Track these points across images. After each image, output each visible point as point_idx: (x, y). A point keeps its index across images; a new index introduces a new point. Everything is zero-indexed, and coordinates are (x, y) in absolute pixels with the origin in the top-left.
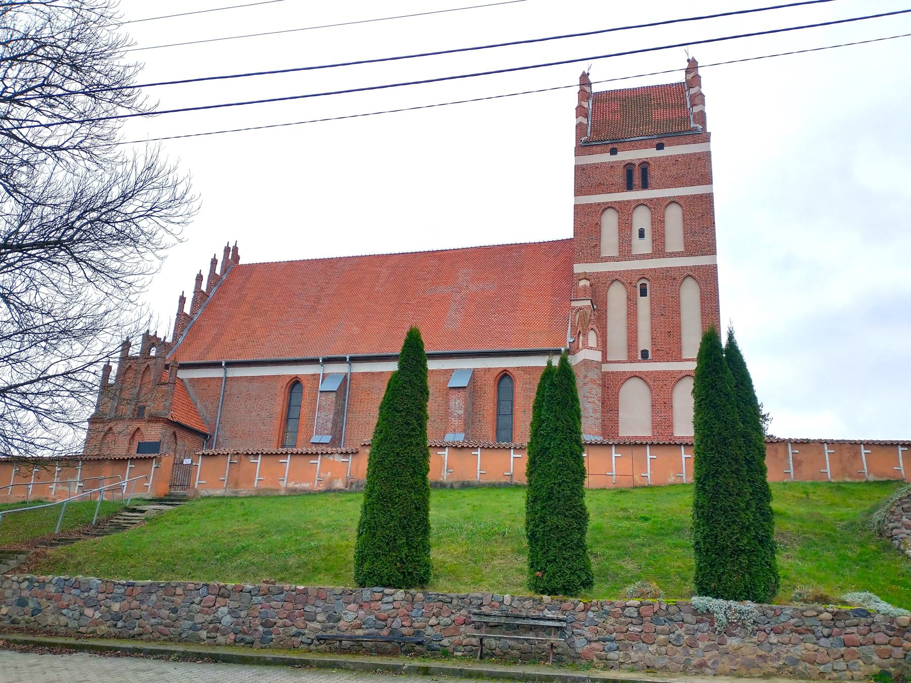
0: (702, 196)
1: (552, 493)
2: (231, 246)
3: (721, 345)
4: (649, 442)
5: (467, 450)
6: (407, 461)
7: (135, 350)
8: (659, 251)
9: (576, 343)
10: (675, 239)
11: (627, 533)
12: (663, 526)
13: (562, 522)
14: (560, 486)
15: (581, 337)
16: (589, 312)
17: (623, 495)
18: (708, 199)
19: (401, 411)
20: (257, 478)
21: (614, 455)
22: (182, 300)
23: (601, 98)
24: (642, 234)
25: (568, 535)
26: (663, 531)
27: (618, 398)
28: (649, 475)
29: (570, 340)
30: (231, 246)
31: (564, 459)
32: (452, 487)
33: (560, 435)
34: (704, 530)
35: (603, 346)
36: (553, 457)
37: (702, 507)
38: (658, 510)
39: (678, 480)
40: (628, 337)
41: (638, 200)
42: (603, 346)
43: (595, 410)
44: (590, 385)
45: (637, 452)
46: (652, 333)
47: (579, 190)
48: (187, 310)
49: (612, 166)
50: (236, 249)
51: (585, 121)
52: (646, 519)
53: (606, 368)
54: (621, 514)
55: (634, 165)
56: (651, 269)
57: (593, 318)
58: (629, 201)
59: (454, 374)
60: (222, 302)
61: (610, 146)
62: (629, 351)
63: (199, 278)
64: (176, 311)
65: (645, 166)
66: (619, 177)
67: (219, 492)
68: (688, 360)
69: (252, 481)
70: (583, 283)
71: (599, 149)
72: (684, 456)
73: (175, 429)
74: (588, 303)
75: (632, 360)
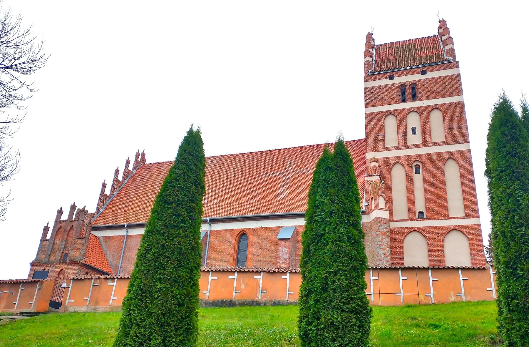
0: (456, 103)
1: (327, 283)
2: (140, 152)
3: (516, 115)
4: (431, 267)
5: (278, 275)
6: (172, 253)
7: (65, 217)
8: (427, 141)
9: (369, 206)
10: (438, 131)
11: (418, 340)
12: (454, 332)
13: (337, 318)
14: (336, 275)
15: (373, 201)
16: (378, 184)
17: (410, 309)
18: (461, 105)
19: (172, 203)
20: (112, 298)
21: (401, 278)
22: (104, 186)
23: (380, 48)
24: (414, 131)
25: (345, 334)
26: (456, 338)
27: (402, 247)
28: (432, 295)
29: (365, 204)
30: (140, 152)
31: (341, 244)
32: (265, 304)
33: (334, 219)
34: (520, 327)
35: (390, 208)
36: (328, 243)
37: (515, 297)
38: (447, 318)
39: (458, 299)
40: (408, 202)
41: (410, 108)
42: (390, 208)
43: (386, 255)
44: (381, 236)
45: (421, 275)
46: (425, 199)
47: (368, 104)
48: (108, 192)
49: (390, 87)
50: (143, 155)
51: (370, 60)
52: (436, 326)
53: (393, 225)
54: (410, 322)
55: (406, 85)
56: (422, 155)
57: (381, 187)
58: (403, 109)
59: (281, 230)
60: (131, 187)
61: (389, 74)
62: (409, 213)
63: (117, 172)
64: (100, 192)
65: (414, 86)
66: (396, 94)
67: (83, 309)
68: (454, 218)
69: (108, 300)
70: (373, 164)
71: (381, 76)
72: (462, 278)
73: (87, 270)
74: (378, 178)
75: (411, 218)
